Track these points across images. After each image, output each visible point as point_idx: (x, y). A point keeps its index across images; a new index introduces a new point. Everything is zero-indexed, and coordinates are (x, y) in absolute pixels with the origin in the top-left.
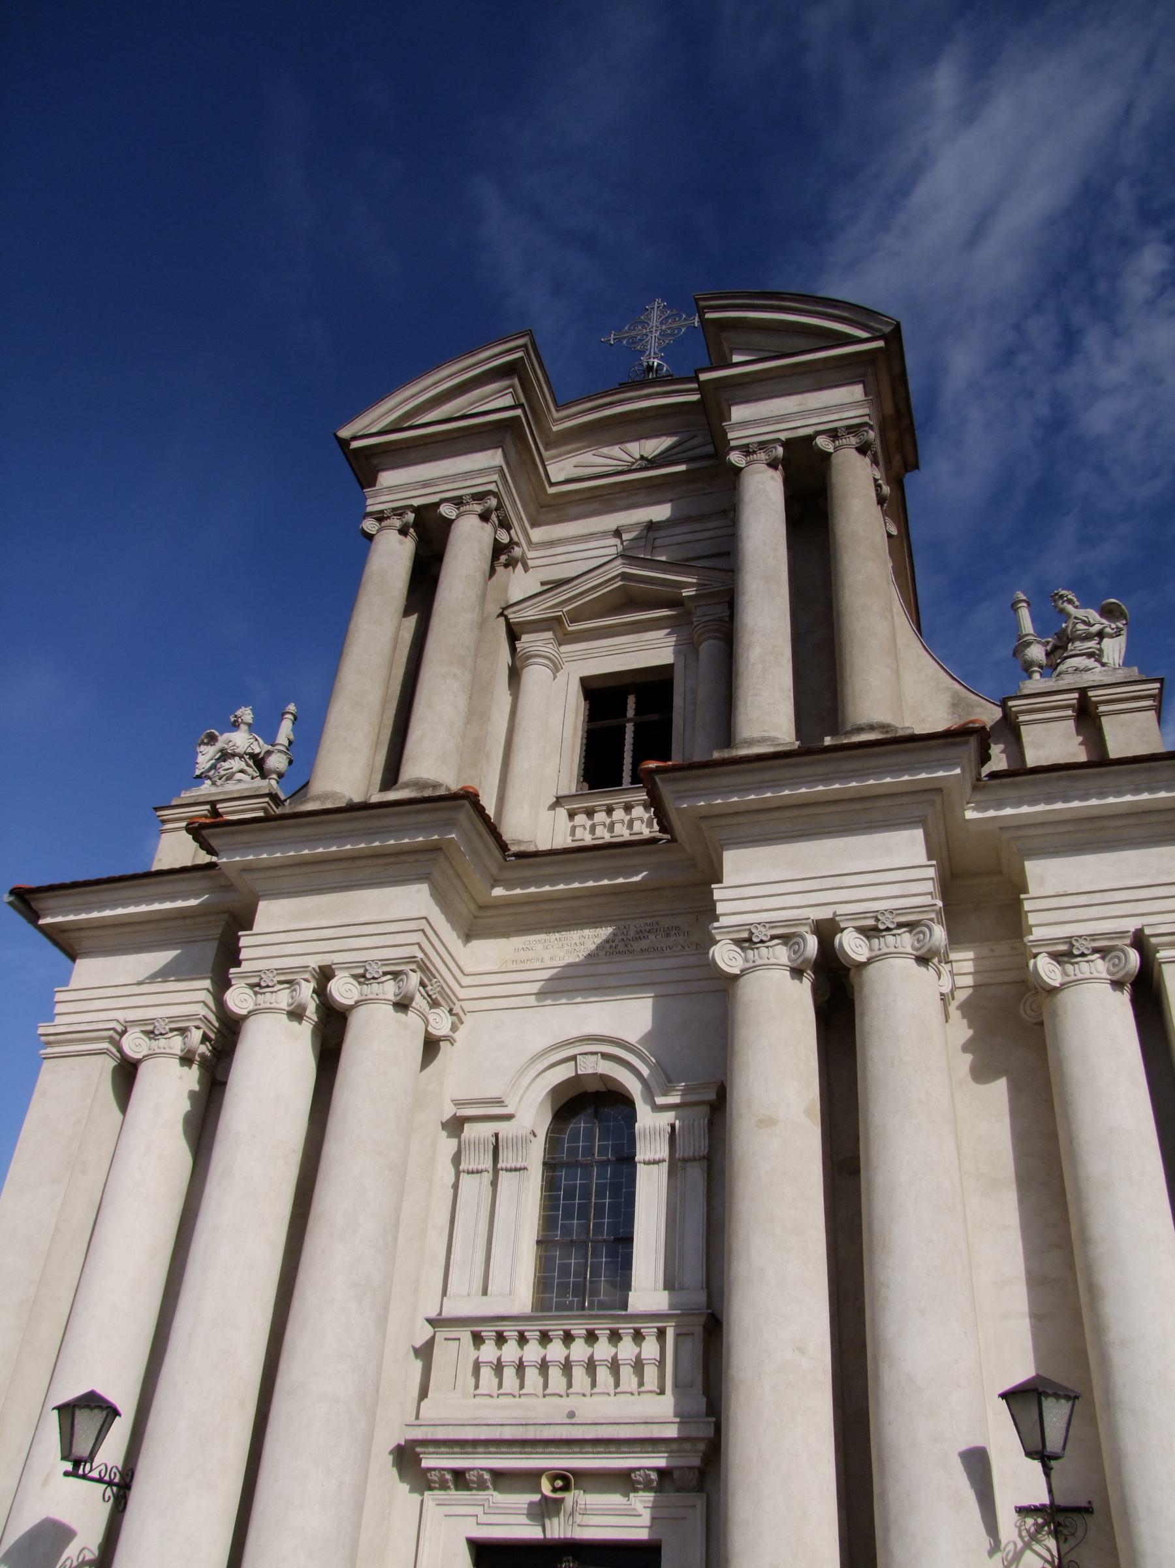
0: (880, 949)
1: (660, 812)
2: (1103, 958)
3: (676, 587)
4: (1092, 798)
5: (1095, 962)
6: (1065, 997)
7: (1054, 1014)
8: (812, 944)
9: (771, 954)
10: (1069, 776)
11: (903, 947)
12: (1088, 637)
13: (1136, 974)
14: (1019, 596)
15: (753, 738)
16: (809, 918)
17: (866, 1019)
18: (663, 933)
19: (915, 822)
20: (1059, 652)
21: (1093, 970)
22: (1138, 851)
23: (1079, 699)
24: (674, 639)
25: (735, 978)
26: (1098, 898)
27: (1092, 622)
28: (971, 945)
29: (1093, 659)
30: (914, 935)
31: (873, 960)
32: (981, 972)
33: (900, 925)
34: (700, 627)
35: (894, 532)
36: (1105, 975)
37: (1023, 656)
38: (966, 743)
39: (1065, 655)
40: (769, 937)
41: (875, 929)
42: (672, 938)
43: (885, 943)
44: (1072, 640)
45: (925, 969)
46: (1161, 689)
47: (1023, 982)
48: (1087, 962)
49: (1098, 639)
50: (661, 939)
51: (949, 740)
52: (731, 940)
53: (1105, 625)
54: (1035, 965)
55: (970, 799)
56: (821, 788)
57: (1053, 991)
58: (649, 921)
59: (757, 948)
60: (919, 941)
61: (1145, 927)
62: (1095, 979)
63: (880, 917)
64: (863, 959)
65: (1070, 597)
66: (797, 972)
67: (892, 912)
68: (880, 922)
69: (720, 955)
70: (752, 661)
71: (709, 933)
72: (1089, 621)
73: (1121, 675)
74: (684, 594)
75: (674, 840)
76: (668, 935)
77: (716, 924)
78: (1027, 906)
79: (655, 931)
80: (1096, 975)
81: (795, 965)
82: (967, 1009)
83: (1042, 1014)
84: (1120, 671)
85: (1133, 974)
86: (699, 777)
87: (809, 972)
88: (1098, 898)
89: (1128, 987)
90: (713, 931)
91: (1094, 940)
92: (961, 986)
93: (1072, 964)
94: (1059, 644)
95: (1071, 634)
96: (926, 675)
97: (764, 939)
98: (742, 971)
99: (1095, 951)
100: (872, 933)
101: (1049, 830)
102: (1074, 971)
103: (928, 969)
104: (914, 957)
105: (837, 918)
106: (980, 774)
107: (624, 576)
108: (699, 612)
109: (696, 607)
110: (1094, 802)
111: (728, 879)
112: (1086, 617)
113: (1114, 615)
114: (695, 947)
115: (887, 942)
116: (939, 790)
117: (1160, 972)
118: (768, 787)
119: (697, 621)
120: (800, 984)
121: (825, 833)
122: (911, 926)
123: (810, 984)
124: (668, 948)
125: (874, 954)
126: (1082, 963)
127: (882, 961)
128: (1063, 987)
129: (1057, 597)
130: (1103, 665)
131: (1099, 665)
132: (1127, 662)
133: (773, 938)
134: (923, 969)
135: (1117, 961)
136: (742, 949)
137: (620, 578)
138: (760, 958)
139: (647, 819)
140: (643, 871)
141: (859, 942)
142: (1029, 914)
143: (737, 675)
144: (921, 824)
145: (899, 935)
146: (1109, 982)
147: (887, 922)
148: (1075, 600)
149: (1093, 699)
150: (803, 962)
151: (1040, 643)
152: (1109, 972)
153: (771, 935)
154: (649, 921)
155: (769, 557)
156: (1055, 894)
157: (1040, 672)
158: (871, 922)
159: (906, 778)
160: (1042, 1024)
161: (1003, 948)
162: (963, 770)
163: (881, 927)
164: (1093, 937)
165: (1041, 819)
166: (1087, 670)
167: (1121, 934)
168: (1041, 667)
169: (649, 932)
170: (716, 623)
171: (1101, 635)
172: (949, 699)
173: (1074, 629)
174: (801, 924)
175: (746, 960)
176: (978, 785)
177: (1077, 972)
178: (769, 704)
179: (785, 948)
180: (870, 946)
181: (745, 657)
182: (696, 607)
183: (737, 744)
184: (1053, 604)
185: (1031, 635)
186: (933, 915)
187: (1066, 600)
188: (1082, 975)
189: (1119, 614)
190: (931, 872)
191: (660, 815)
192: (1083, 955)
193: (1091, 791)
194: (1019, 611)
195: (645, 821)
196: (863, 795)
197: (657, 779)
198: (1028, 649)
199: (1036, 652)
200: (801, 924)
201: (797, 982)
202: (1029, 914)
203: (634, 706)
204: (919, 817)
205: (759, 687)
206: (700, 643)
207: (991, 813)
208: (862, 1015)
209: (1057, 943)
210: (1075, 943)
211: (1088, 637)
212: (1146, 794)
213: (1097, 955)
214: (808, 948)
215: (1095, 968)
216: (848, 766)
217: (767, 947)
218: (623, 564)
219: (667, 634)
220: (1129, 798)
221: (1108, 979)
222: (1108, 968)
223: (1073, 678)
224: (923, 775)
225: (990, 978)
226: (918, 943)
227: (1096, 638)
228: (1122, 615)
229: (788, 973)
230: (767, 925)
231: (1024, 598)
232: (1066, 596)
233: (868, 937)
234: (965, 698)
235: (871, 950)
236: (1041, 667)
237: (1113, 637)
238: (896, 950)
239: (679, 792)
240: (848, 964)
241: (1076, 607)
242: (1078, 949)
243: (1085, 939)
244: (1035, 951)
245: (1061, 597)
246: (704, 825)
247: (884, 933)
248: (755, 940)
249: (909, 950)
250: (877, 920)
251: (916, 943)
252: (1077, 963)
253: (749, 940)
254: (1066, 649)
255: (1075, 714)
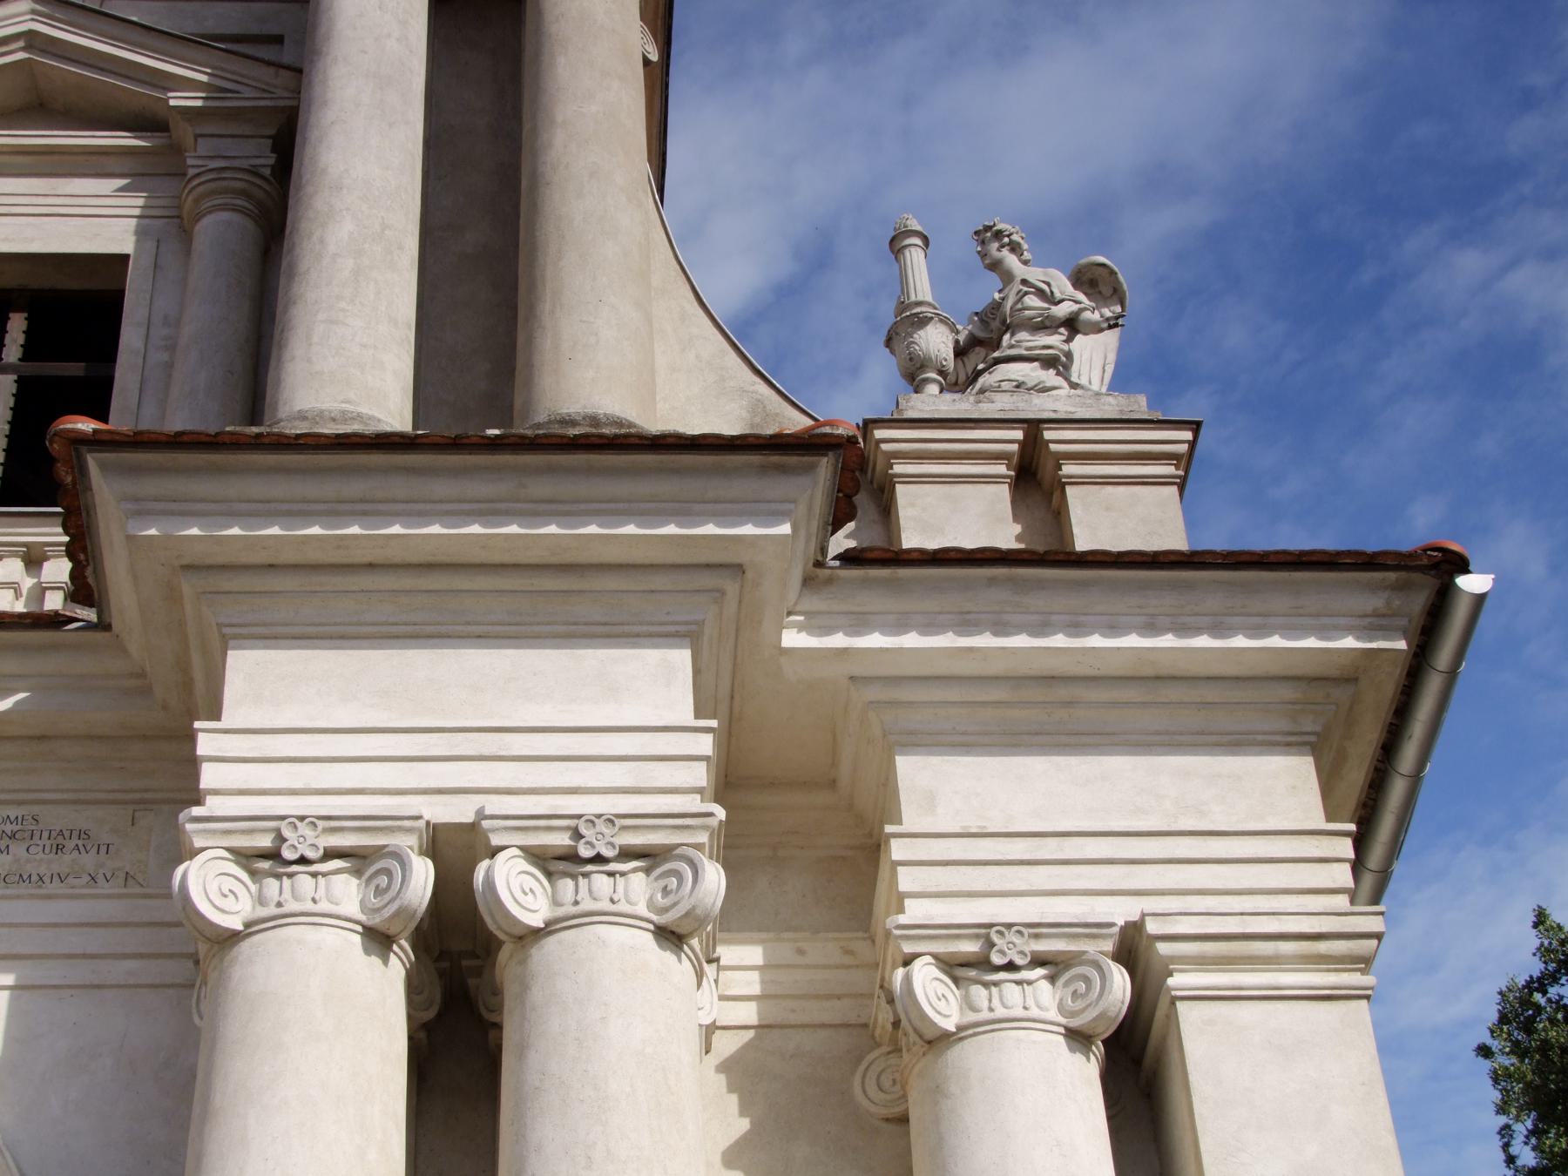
0: (576, 903)
1: (84, 550)
2: (1052, 979)
3: (155, 86)
4: (1202, 634)
5: (1035, 984)
6: (963, 1056)
7: (937, 1091)
8: (421, 878)
9: (321, 892)
10: (1011, 580)
11: (628, 902)
12: (1046, 325)
13: (1121, 1017)
14: (908, 222)
15: (322, 412)
16: (419, 818)
17: (533, 1058)
18: (48, 843)
19: (676, 635)
20: (980, 351)
21: (1030, 1002)
22: (1138, 758)
23: (1023, 444)
24: (140, 202)
25: (231, 938)
26: (1050, 849)
27: (1058, 295)
28: (755, 935)
29: (1052, 372)
30: (657, 879)
31: (558, 926)
32: (776, 997)
33: (627, 854)
34: (203, 179)
35: (654, 57)
36: (1053, 1014)
37: (908, 347)
38: (810, 469)
39: (996, 354)
40: (321, 852)
41: (572, 857)
42: (67, 858)
43: (590, 891)
44: (1008, 328)
45: (673, 958)
46: (1193, 444)
47: (865, 1026)
48: (1018, 983)
49: (1066, 333)
50: (41, 855)
51: (775, 459)
52: (521, 848)
53: (1082, 306)
54: (908, 980)
55: (796, 604)
56: (476, 529)
57: (941, 1041)
58: (13, 812)
59: (290, 876)
60: (665, 891)
61: (1147, 919)
62: (1034, 1020)
63: (583, 830)
64: (536, 921)
65: (1015, 237)
66: (378, 939)
67: (610, 820)
68: (583, 841)
69: (201, 881)
70: (332, 248)
71: (177, 830)
72: (1052, 292)
73: (1112, 406)
74: (172, 103)
75: (103, 625)
76: (59, 848)
77: (196, 811)
78: (898, 850)
79: (28, 834)
80: (1034, 1012)
81: (376, 921)
82: (739, 1072)
83: (904, 1097)
84: (1111, 399)
85: (1117, 1016)
86: (196, 471)
87: (403, 942)
88: (1050, 849)
89: (1098, 1048)
90: (189, 827)
91: (1037, 936)
92: (725, 1024)
93: (986, 985)
94: (981, 334)
95: (1011, 316)
96: (697, 357)
97: (310, 854)
98: (248, 925)
99: (1038, 961)
100: (562, 866)
101: (953, 694)
102: (990, 1001)
103: (680, 960)
104: (651, 927)
105: (486, 824)
106: (823, 550)
107: (31, 40)
108: (204, 147)
109: (197, 136)
110: (1059, 641)
111: (232, 715)
112: (1044, 282)
113: (1100, 293)
114: (121, 881)
115: (594, 889)
116: (738, 569)
117: (1172, 1016)
118: (353, 513)
119: (193, 166)
120: (382, 967)
121: (468, 636)
122: (649, 857)
123: (403, 973)
124: (56, 878)
125: (560, 912)
126: (1008, 984)
127: (579, 929)
128: (963, 1034)
129: (989, 234)
130: (1074, 386)
131: (1065, 384)
132: (1121, 381)
133: (330, 854)
134: (669, 957)
135: (1082, 986)
136: (253, 873)
137: (21, 44)
138: (295, 896)
139: (30, 589)
140: (16, 691)
141: (530, 882)
142: (900, 869)
143: (291, 275)
144: (687, 641)
145: (623, 874)
146: (1062, 1030)
147: (598, 842)
148: (1025, 246)
149: (1053, 447)
150: (397, 914)
151: (947, 324)
152: (1061, 1009)
153: (325, 849)
154: (13, 812)
155: (389, 36)
156: (958, 830)
157: (941, 384)
158: (562, 840)
159: (671, 529)
160: (903, 1120)
161: (825, 949)
162: (795, 528)
163: (585, 852)
164: (1035, 929)
165: (943, 668)
166: (1045, 390)
167: (1096, 928)
168: (942, 372)
169: (13, 836)
170: (240, 176)
171: (1072, 325)
172: (744, 414)
173: (1019, 306)
174: (400, 829)
175: (261, 900)
176: (816, 575)
177: (996, 1002)
178: (364, 346)
179: (354, 881)
180: (553, 896)
181: (315, 238)
182: (197, 136)
183: (282, 420)
184: (979, 249)
185: (929, 304)
186: (703, 838)
187: (1008, 245)
188: (1005, 1011)
189: (1111, 292)
190: (705, 744)
191: (82, 557)
192: (1011, 967)
193: (1054, 618)
194: (907, 252)
195: (25, 592)
196: (568, 558)
197: (92, 461)
198: (921, 333)
199: (936, 342)
200: (400, 829)
201: (375, 961)
202: (900, 869)
203: (21, 339)
204: (687, 623)
205: (343, 305)
206: (198, 218)
207: (838, 640)
208: (522, 1049)
209: (958, 937)
210: (995, 938)
211: (1047, 323)
212: (1170, 636)
213: (1040, 972)
214: (413, 882)
215: (1035, 997)
216: (541, 488)
217: (314, 875)
218: (33, 12)
219: (121, 189)
220: (1133, 641)
221: (1059, 1025)
222: (1061, 1000)
223: (1011, 400)
224: (710, 529)
225: (793, 1011)
226: (663, 898)
227: (1062, 330)
228: (1117, 295)
229: (357, 939)
230: (321, 824)
231: (919, 228)
232: (1008, 236)
233: (549, 875)
234: (777, 414)
235: (556, 902)
236: (942, 372)
237: (1101, 330)
238: (613, 908)
239: (136, 500)
240: (500, 928)
241: (1026, 263)
242: (1002, 952)
243: (1019, 932)
244: (908, 948)
245: (999, 235)
246: (188, 587)
247: (589, 868)
248: (288, 854)
249: (642, 909)
250: (577, 835)
251: (659, 896)
252: (996, 984)
253: (273, 855)
254: (997, 345)
255: (1012, 473)
